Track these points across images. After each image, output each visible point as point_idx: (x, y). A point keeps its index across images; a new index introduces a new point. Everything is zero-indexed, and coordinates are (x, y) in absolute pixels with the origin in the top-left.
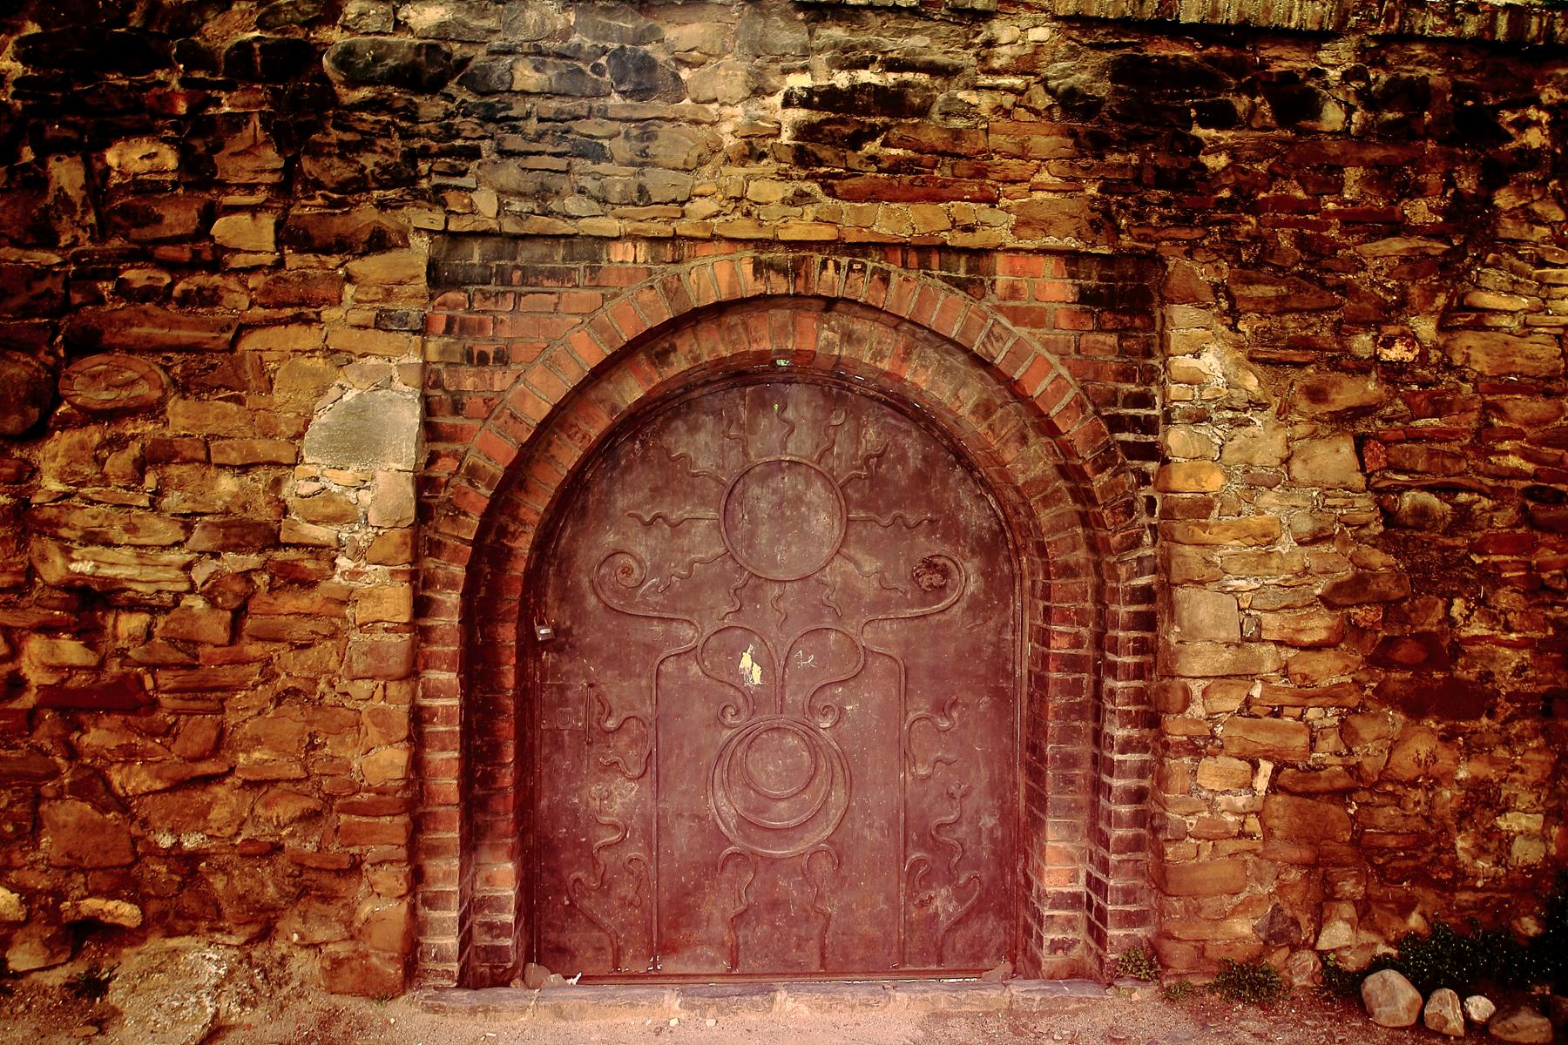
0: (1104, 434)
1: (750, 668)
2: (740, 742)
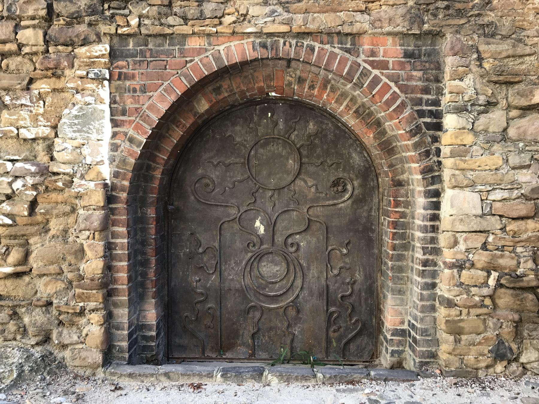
0: (415, 119)
1: (260, 227)
2: (255, 259)
